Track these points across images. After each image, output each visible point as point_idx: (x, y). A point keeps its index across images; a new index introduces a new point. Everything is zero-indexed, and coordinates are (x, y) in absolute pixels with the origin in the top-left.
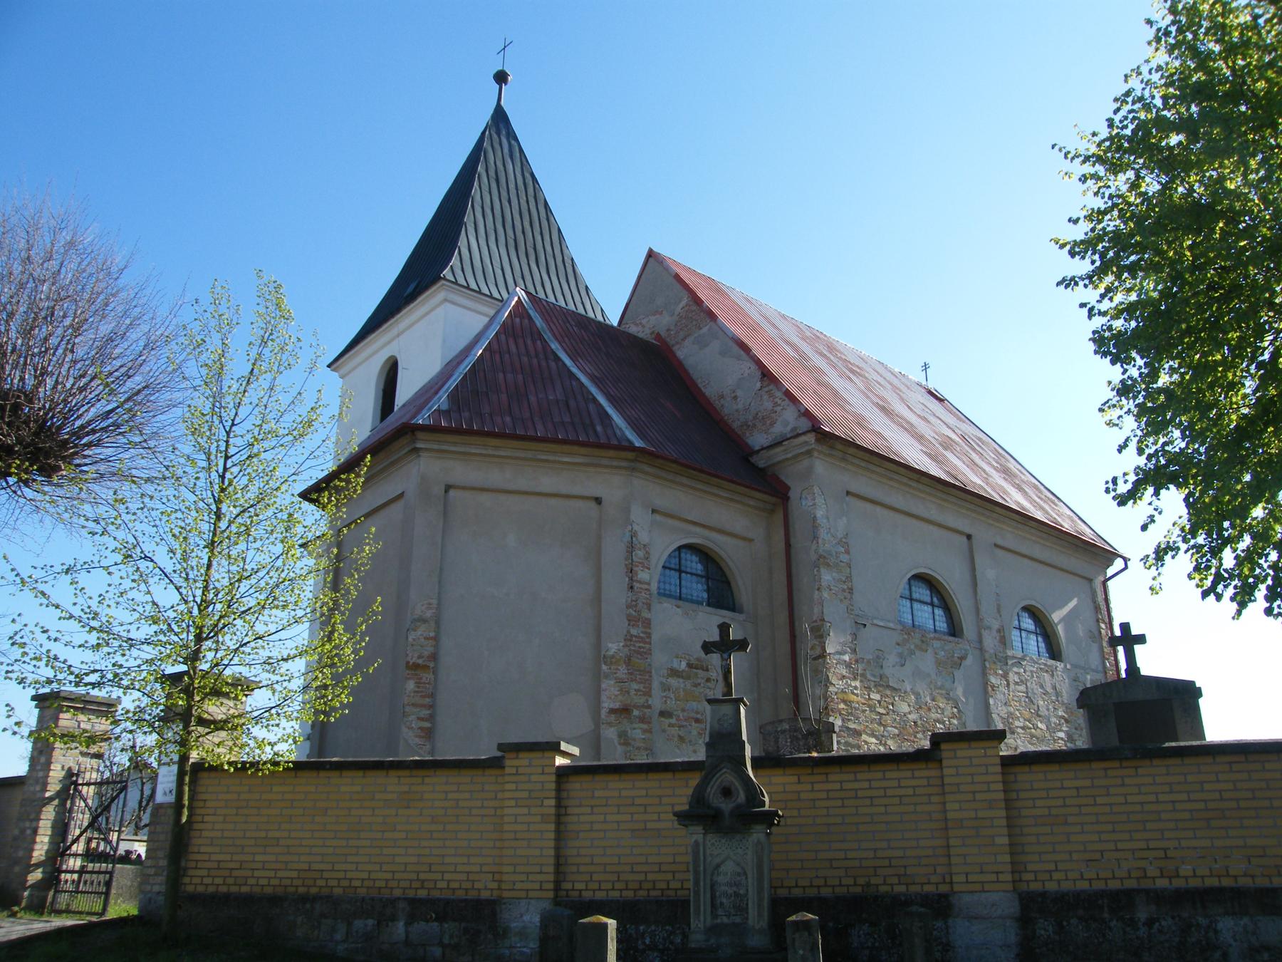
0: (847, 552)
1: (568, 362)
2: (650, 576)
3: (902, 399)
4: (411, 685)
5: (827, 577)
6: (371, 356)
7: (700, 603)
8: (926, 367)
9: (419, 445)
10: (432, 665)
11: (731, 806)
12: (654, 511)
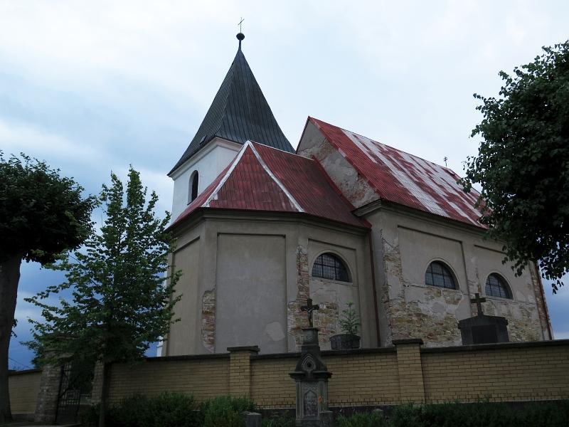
0: (399, 253)
1: (270, 174)
2: (308, 268)
3: (430, 177)
4: (205, 321)
5: (390, 265)
6: (186, 171)
7: (332, 279)
8: (446, 159)
9: (205, 216)
10: (213, 312)
11: (311, 370)
12: (309, 239)
